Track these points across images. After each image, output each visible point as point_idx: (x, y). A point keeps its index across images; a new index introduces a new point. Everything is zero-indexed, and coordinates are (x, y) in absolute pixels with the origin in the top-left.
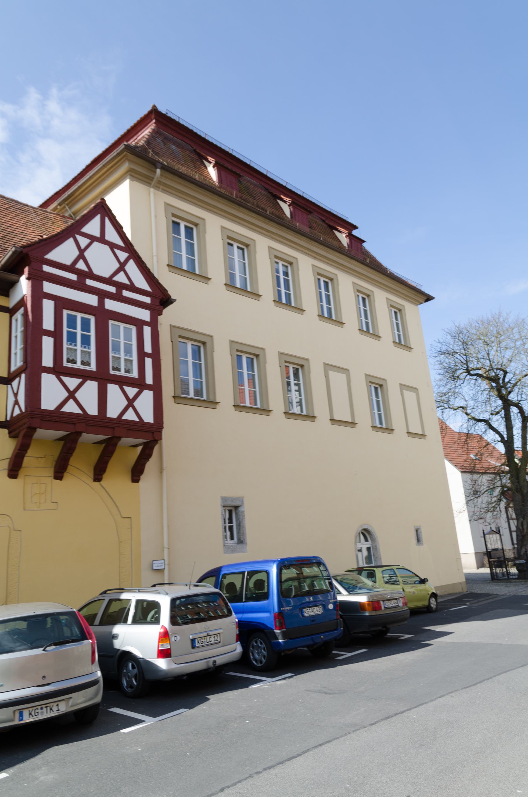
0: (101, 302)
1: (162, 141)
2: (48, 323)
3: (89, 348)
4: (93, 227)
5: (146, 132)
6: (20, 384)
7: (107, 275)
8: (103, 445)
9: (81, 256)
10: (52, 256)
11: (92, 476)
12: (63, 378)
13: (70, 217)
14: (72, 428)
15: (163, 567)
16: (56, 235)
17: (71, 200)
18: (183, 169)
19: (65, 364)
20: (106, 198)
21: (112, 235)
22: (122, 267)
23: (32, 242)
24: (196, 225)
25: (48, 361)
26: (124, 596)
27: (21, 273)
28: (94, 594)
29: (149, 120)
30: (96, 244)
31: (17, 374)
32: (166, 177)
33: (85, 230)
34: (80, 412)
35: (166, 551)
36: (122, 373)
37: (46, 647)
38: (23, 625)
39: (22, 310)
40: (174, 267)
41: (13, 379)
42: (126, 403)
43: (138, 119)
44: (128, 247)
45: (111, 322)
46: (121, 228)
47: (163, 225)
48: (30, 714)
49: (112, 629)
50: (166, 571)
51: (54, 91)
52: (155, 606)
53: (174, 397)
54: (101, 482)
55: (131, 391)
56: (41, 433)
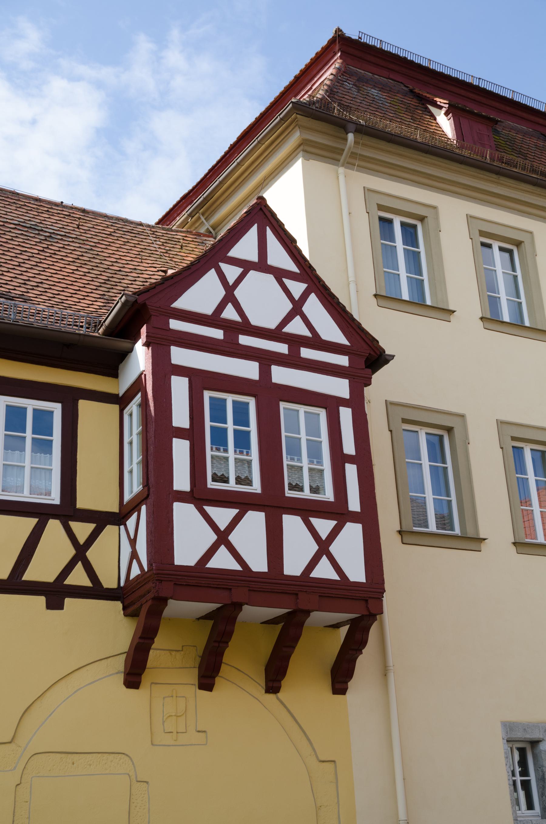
0: (265, 373)
2: (181, 417)
4: (246, 248)
7: (272, 325)
9: (229, 297)
10: (183, 303)
11: (263, 684)
21: (277, 256)
22: (297, 309)
25: (182, 481)
30: (252, 274)
36: (307, 494)
44: (307, 272)
51: (175, 34)
54: (278, 694)
55: (324, 527)
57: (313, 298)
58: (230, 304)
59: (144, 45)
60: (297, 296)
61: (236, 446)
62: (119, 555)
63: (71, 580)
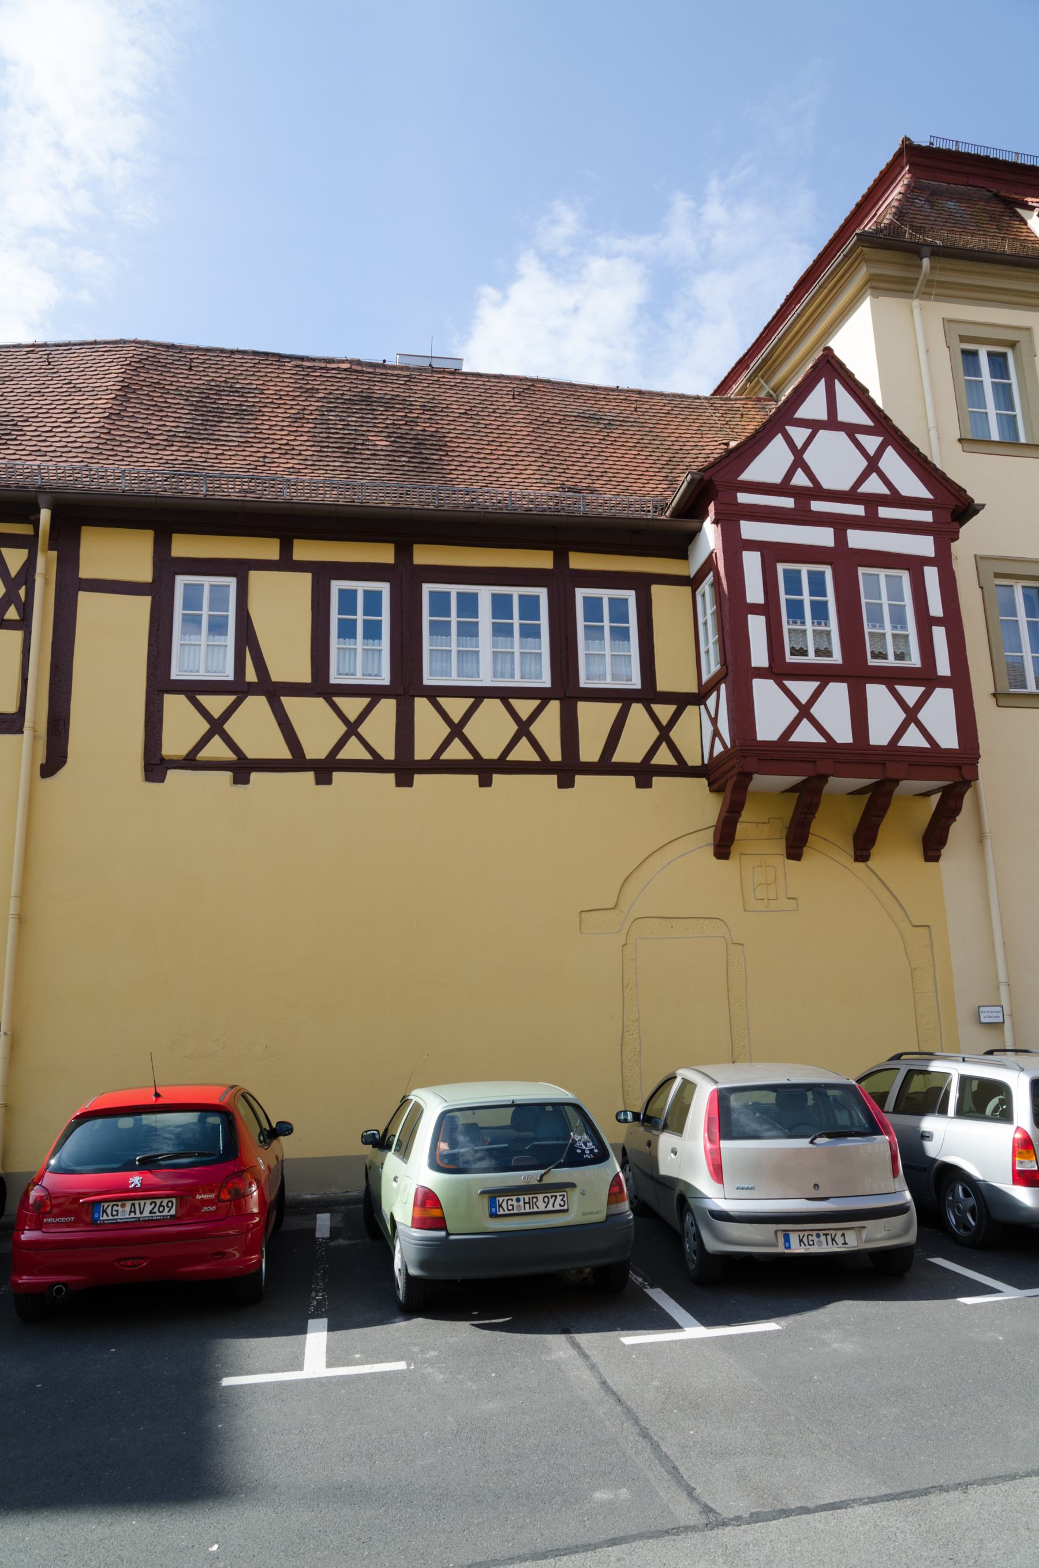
0: (841, 538)
1: (927, 201)
2: (755, 594)
3: (826, 625)
4: (814, 407)
5: (895, 193)
6: (720, 702)
7: (845, 485)
8: (867, 796)
9: (799, 462)
11: (852, 853)
12: (788, 684)
13: (770, 398)
14: (810, 768)
15: (1000, 1020)
16: (753, 437)
17: (768, 368)
18: (975, 242)
19: (789, 659)
20: (832, 344)
21: (850, 411)
22: (873, 465)
23: (715, 459)
24: (1013, 345)
25: (759, 657)
26: (936, 1066)
27: (704, 515)
28: (879, 1058)
29: (899, 169)
30: (822, 433)
31: (713, 686)
32: (942, 269)
33: (802, 413)
34: (821, 740)
35: (1003, 990)
36: (891, 661)
37: (815, 1138)
38: (771, 1098)
39: (710, 577)
40: (973, 441)
41: (707, 695)
42: (902, 716)
43: (876, 175)
44: (882, 424)
45: (861, 571)
46: (865, 391)
47: (943, 363)
48: (801, 1241)
49: (920, 1121)
50: (1007, 1026)
51: (714, 185)
52: (1001, 1089)
53: (994, 695)
55: (911, 694)
56: (761, 782)
57: (890, 451)
58: (799, 470)
59: (681, 203)
60: (871, 452)
61: (893, 621)
62: (702, 734)
63: (656, 760)
